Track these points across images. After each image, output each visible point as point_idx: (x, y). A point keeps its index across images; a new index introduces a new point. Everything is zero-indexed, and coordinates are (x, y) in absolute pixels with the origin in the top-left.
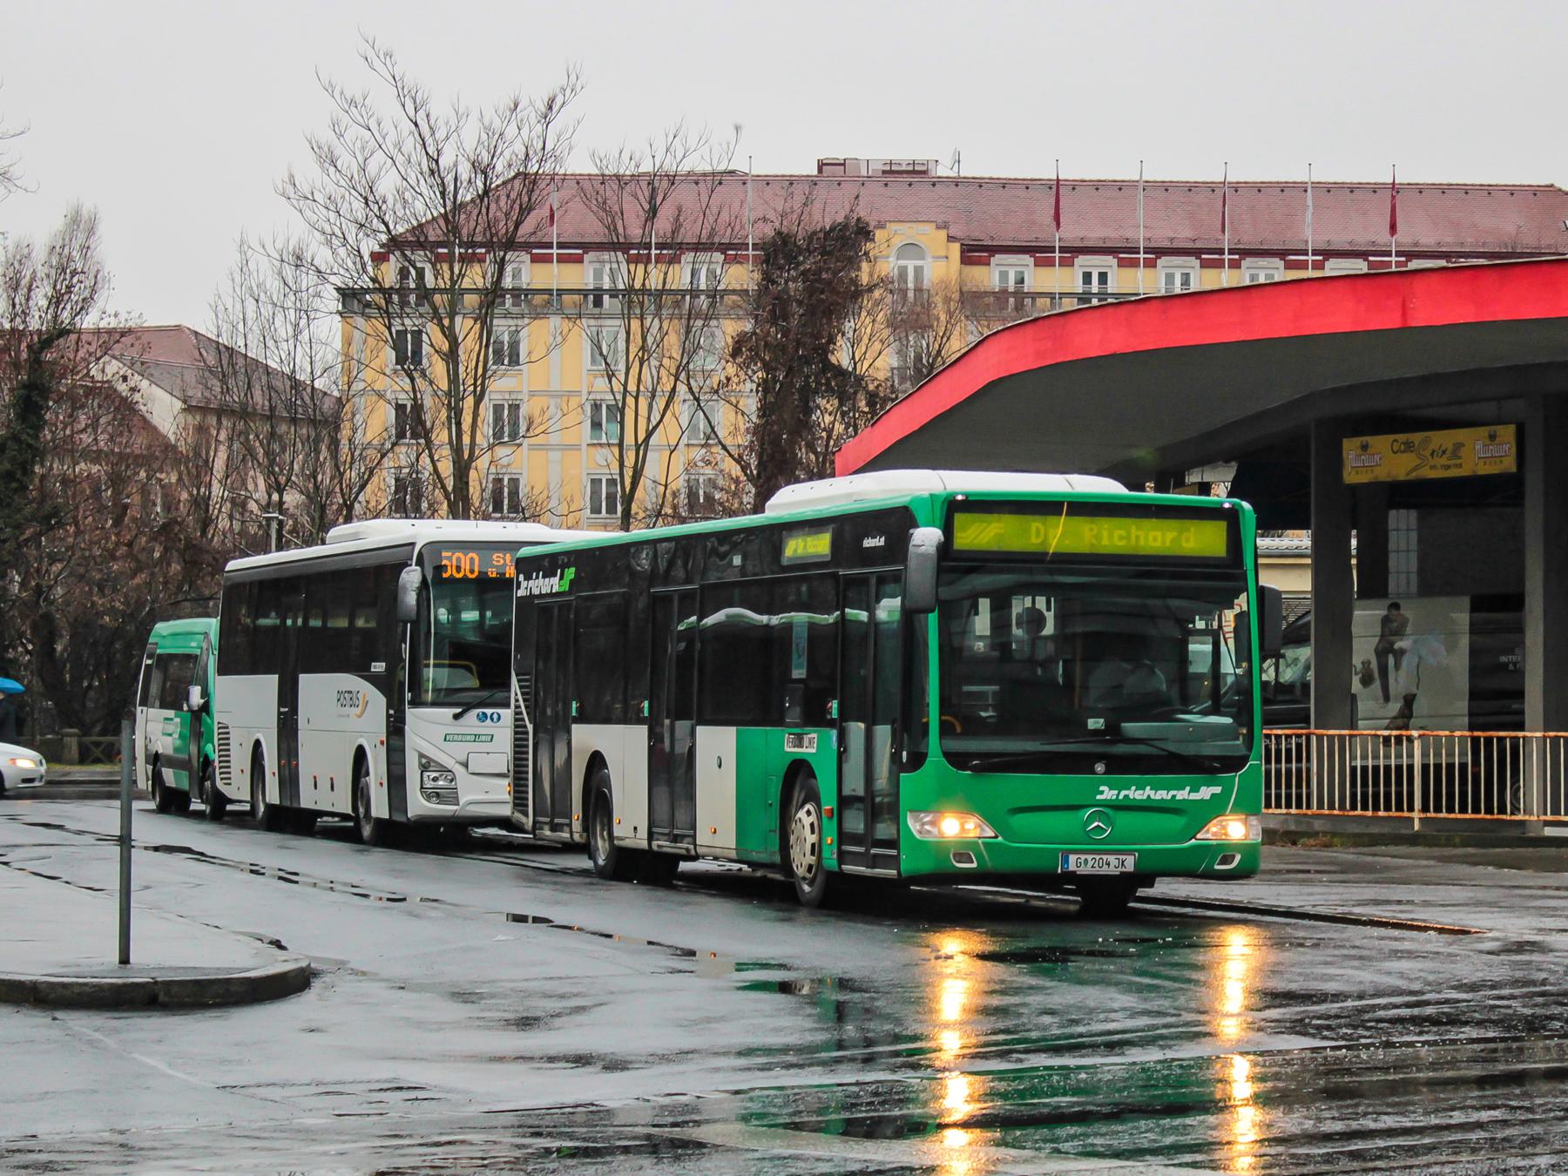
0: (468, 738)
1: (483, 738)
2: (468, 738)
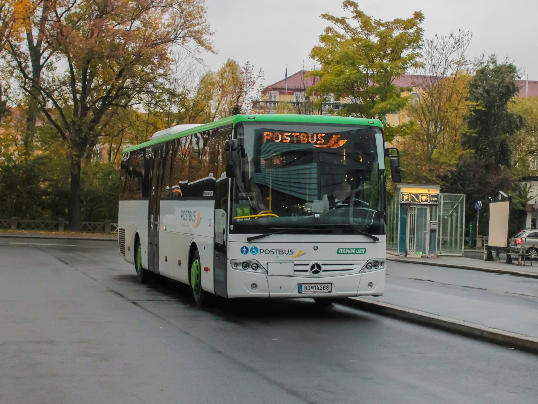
0: (352, 251)
1: (360, 251)
2: (352, 251)
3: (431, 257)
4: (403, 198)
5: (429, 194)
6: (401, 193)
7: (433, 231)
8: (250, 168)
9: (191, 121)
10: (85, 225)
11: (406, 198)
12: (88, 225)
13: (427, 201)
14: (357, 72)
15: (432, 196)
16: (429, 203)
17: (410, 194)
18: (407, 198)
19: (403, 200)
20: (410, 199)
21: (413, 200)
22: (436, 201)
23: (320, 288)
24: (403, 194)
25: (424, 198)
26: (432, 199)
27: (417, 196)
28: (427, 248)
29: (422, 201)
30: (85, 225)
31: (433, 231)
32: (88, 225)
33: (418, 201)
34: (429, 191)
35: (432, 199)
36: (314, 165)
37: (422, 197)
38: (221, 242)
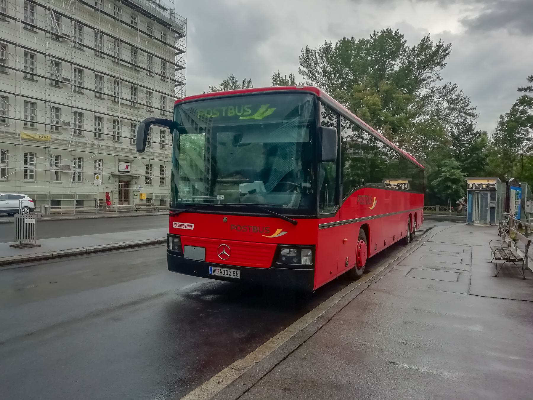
3: (492, 226)
4: (469, 186)
5: (489, 183)
6: (468, 183)
7: (492, 209)
8: (291, 154)
9: (25, 52)
10: (430, 207)
11: (471, 186)
12: (442, 208)
13: (486, 188)
14: (393, 69)
15: (491, 185)
16: (488, 189)
17: (474, 183)
18: (472, 187)
19: (469, 188)
20: (474, 187)
21: (476, 187)
22: (494, 188)
23: (223, 272)
24: (469, 184)
25: (484, 186)
26: (490, 186)
27: (479, 185)
28: (488, 220)
29: (483, 188)
30: (430, 207)
31: (492, 209)
32: (442, 208)
33: (480, 188)
34: (488, 181)
35: (490, 186)
36: (469, 181)
37: (483, 185)
38: (61, 208)
